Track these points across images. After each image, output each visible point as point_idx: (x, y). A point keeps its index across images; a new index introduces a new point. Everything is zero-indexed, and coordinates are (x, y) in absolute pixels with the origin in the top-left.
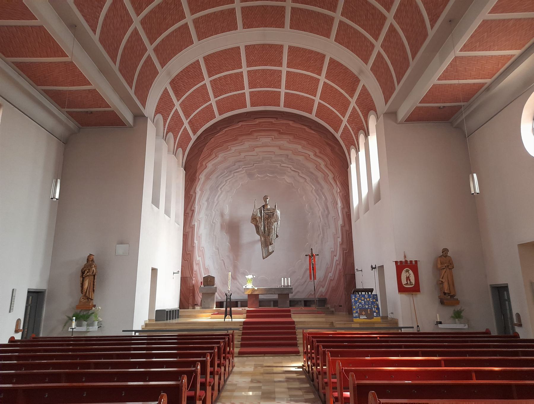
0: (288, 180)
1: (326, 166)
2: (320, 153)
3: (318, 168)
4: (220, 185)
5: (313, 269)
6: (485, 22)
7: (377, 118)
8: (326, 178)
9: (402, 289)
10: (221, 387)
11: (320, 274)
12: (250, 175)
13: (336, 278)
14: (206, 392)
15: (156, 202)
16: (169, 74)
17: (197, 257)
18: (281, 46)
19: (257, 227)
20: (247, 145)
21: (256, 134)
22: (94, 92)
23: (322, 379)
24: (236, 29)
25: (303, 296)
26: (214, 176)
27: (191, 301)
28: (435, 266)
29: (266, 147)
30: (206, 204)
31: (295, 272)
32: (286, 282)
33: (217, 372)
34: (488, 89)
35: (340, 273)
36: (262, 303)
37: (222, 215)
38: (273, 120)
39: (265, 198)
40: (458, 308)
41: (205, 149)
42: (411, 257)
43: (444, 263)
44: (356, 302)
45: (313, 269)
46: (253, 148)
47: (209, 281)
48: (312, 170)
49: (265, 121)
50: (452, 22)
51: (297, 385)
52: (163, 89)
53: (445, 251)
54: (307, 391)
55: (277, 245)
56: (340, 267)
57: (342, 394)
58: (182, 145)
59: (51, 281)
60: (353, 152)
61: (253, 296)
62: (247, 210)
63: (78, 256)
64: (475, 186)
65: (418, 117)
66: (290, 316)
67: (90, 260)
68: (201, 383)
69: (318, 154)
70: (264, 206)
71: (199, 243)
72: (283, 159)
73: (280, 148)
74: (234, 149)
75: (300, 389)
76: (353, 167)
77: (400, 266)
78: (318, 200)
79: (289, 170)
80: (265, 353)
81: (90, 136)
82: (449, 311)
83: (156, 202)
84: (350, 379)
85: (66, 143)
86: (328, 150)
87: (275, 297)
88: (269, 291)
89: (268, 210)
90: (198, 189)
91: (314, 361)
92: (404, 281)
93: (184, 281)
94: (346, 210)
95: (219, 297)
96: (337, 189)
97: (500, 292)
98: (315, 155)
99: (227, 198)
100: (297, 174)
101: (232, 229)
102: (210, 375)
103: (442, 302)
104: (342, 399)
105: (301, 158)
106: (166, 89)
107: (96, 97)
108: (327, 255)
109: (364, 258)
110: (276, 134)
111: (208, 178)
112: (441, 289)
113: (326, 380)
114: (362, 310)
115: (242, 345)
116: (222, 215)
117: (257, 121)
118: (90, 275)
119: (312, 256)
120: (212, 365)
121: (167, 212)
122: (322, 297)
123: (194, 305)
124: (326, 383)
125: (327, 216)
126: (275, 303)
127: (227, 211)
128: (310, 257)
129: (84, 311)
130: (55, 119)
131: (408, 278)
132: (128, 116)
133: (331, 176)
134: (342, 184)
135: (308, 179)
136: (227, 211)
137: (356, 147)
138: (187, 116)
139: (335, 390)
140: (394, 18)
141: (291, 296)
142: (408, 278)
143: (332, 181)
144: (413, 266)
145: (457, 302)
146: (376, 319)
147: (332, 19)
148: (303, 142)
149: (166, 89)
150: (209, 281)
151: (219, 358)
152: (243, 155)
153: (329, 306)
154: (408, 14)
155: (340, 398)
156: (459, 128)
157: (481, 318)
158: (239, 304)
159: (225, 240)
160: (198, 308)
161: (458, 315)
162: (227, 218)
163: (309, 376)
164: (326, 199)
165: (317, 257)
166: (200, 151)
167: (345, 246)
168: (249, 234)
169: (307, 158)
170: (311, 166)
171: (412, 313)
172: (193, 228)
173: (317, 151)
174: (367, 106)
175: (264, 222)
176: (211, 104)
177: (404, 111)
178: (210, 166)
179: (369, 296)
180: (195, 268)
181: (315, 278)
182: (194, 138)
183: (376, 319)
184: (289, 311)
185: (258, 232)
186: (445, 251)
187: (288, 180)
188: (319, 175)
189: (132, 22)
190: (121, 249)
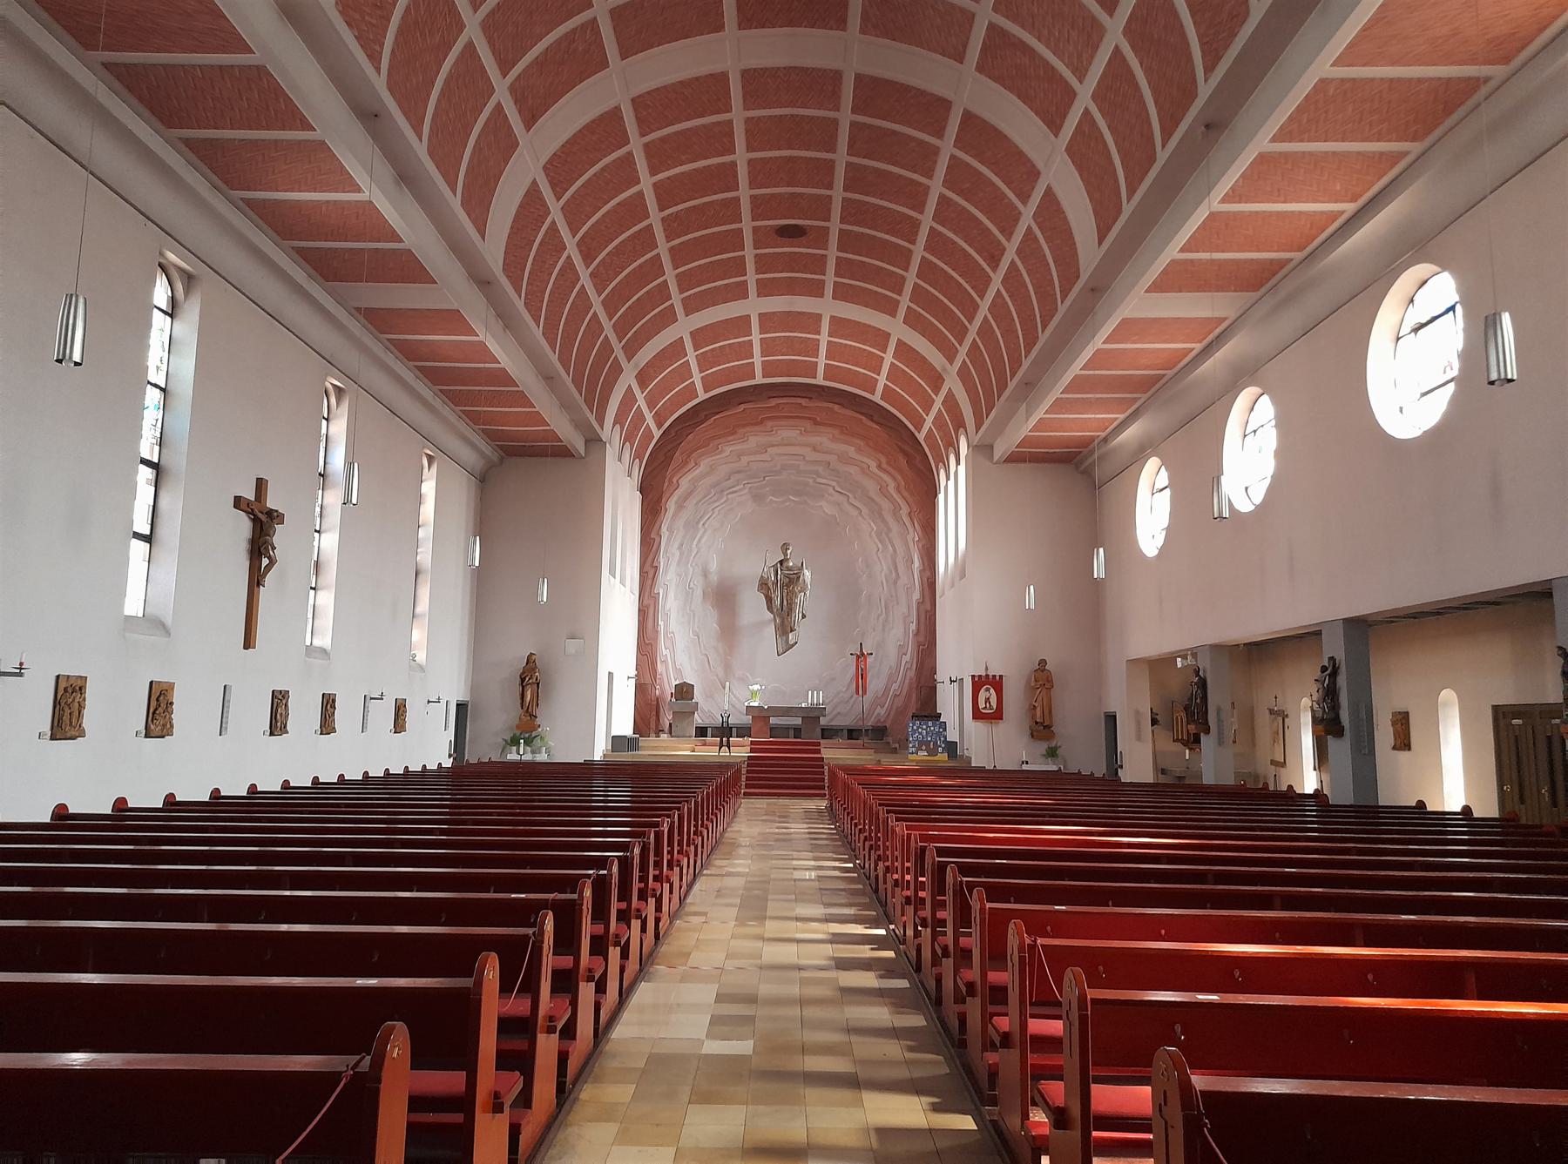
0: (829, 509)
1: (898, 489)
2: (888, 463)
5: (861, 675)
6: (1262, 158)
8: (896, 509)
9: (978, 715)
10: (573, 1065)
11: (875, 684)
12: (758, 498)
14: (606, 960)
15: (612, 573)
16: (636, 365)
17: (663, 650)
18: (820, 316)
19: (769, 600)
20: (753, 441)
21: (770, 424)
22: (260, 73)
23: (987, 1018)
24: (720, 28)
25: (846, 721)
26: (692, 501)
27: (653, 725)
28: (1028, 682)
29: (787, 445)
30: (677, 554)
32: (814, 698)
33: (617, 936)
34: (1105, 440)
36: (774, 731)
38: (804, 402)
39: (785, 548)
42: (995, 671)
43: (1042, 679)
44: (914, 732)
45: (861, 675)
46: (763, 449)
47: (684, 691)
48: (872, 494)
49: (789, 399)
50: (1213, 126)
51: (881, 1014)
52: (527, 183)
53: (1043, 662)
54: (886, 969)
55: (806, 632)
56: (912, 673)
57: (1024, 1026)
58: (638, 455)
59: (474, 688)
61: (760, 715)
62: (755, 564)
63: (514, 654)
64: (1099, 571)
65: (1028, 456)
66: (819, 752)
67: (530, 659)
68: (592, 937)
69: (884, 466)
70: (781, 562)
71: (666, 626)
72: (820, 469)
73: (815, 449)
74: (728, 450)
75: (880, 993)
76: (941, 497)
78: (880, 552)
80: (779, 795)
81: (519, 469)
82: (1042, 747)
83: (612, 573)
84: (975, 905)
85: (485, 481)
86: (903, 462)
87: (798, 721)
88: (787, 712)
89: (789, 569)
90: (664, 529)
91: (927, 913)
92: (982, 704)
93: (641, 690)
95: (698, 720)
96: (914, 535)
98: (879, 467)
99: (718, 538)
101: (723, 598)
102: (554, 990)
104: (1023, 1043)
105: (853, 470)
106: (534, 182)
107: (369, 222)
108: (892, 651)
109: (956, 661)
110: (808, 424)
111: (680, 506)
112: (1034, 716)
113: (1004, 1024)
114: (922, 744)
115: (747, 786)
116: (705, 574)
117: (773, 402)
118: (531, 681)
119: (861, 656)
120: (600, 913)
121: (623, 582)
123: (658, 732)
124: (970, 986)
125: (895, 583)
126: (797, 731)
127: (714, 567)
129: (526, 730)
130: (471, 450)
131: (987, 700)
132: (579, 445)
133: (905, 510)
134: (923, 527)
135: (865, 511)
136: (714, 567)
138: (643, 388)
139: (999, 1009)
140: (1094, 97)
141: (823, 721)
142: (987, 700)
143: (906, 519)
144: (997, 683)
147: (936, 151)
149: (534, 182)
150: (684, 691)
151: (624, 895)
152: (745, 459)
153: (890, 739)
154: (1152, 29)
155: (1017, 1037)
156: (1088, 473)
157: (1085, 758)
160: (664, 736)
161: (1052, 753)
162: (714, 578)
163: (830, 808)
165: (870, 660)
166: (669, 458)
167: (921, 639)
168: (753, 608)
169: (865, 471)
170: (871, 487)
171: (993, 747)
172: (656, 598)
173: (884, 460)
175: (781, 591)
176: (640, 194)
177: (1002, 448)
178: (685, 483)
180: (660, 668)
181: (864, 692)
182: (657, 434)
185: (770, 608)
186: (1043, 662)
187: (829, 509)
188: (886, 505)
189: (461, 27)
190: (572, 646)
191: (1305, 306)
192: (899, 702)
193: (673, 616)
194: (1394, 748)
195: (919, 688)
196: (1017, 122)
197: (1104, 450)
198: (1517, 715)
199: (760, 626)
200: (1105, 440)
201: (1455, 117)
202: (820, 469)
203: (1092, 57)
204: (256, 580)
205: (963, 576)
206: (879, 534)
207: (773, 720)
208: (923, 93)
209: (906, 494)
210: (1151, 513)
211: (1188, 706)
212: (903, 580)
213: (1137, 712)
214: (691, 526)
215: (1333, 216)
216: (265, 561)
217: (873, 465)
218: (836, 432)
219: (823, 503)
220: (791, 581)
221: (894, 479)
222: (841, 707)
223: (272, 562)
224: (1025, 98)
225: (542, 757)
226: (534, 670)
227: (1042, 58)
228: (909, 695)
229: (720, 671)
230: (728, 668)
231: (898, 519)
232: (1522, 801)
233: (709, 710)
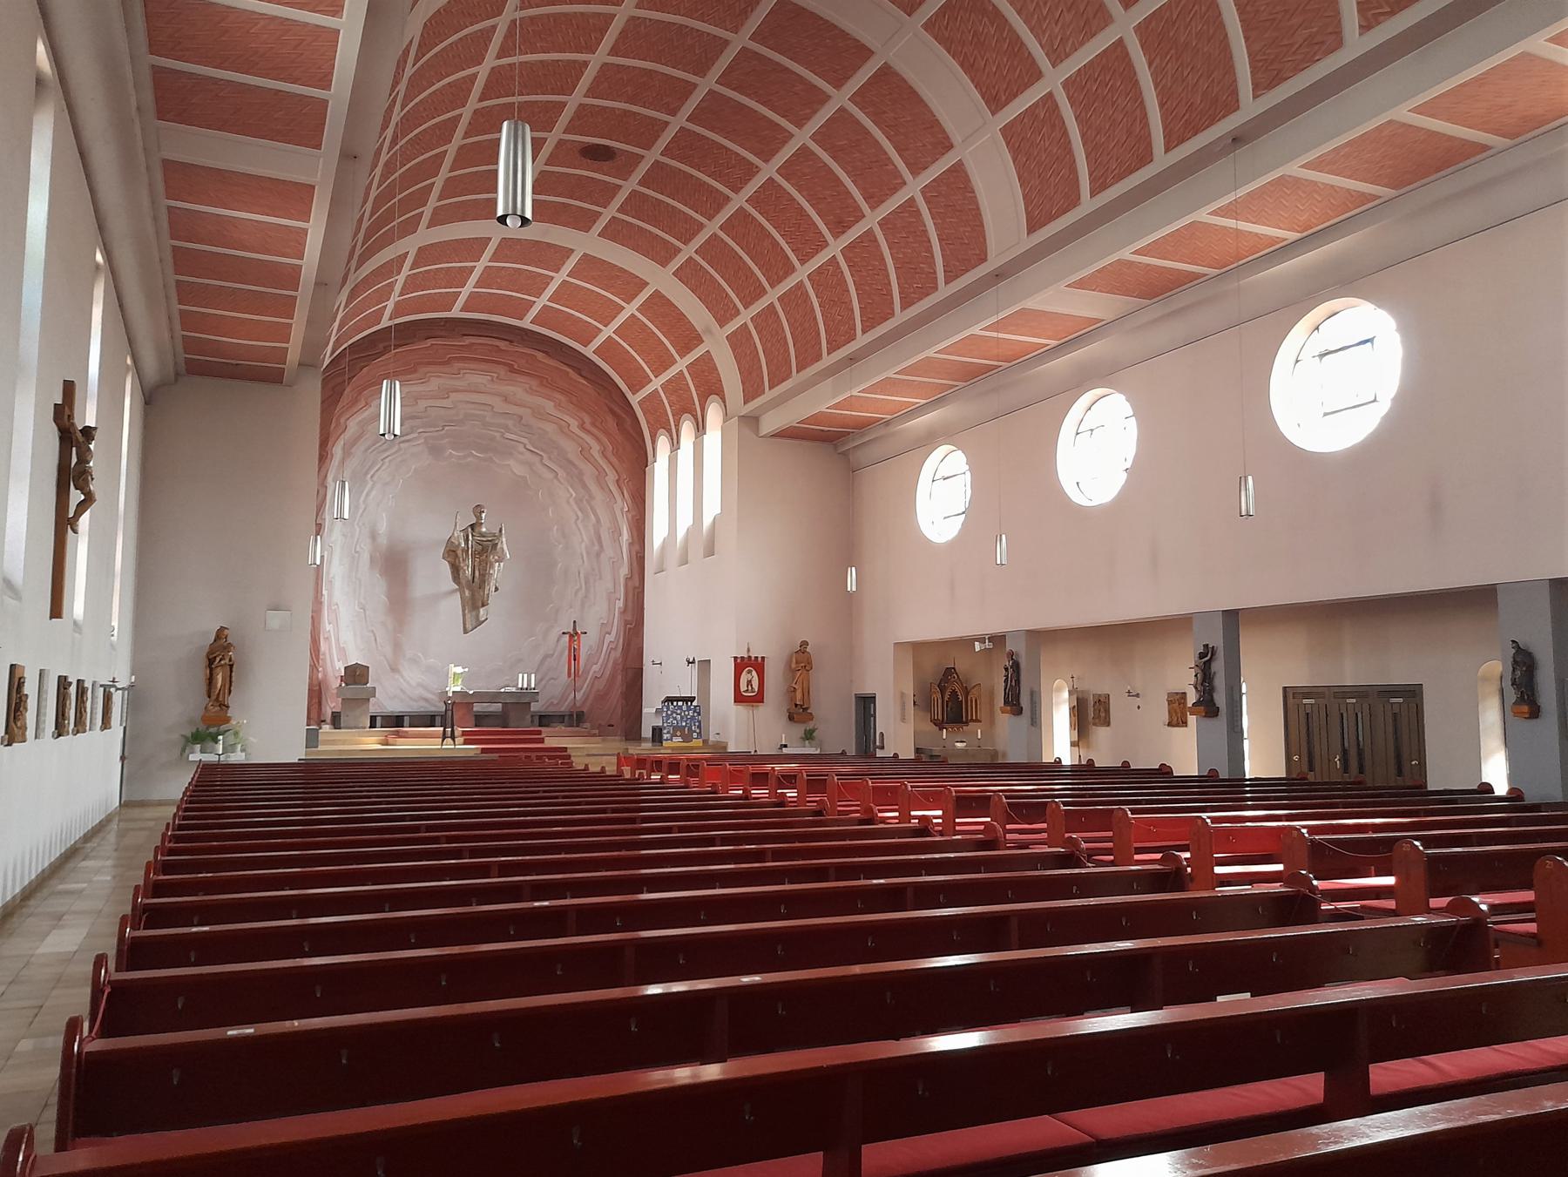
0: (519, 470)
2: (593, 424)
3: (584, 452)
4: (370, 468)
7: (727, 417)
8: (600, 477)
9: (739, 698)
12: (435, 451)
13: (608, 672)
17: (327, 626)
19: (456, 570)
20: (435, 384)
28: (789, 663)
29: (478, 392)
31: (520, 660)
35: (615, 663)
37: (374, 536)
38: (503, 345)
39: (478, 510)
40: (810, 725)
41: (348, 390)
43: (801, 661)
46: (446, 393)
47: (356, 675)
48: (571, 456)
53: (804, 644)
55: (496, 609)
60: (663, 443)
62: (435, 528)
64: (851, 585)
67: (220, 634)
69: (588, 425)
71: (330, 595)
72: (510, 423)
73: (506, 400)
77: (741, 665)
78: (577, 518)
79: (521, 448)
86: (611, 423)
88: (493, 697)
92: (743, 687)
94: (637, 547)
95: (374, 708)
96: (622, 505)
97: (866, 704)
98: (582, 427)
100: (537, 459)
101: (394, 565)
103: (791, 718)
105: (549, 428)
110: (502, 371)
111: (347, 453)
112: (792, 699)
116: (374, 536)
117: (468, 341)
118: (220, 663)
122: (552, 709)
125: (598, 555)
127: (383, 528)
128: (571, 636)
131: (749, 682)
133: (611, 477)
134: (633, 497)
135: (561, 473)
136: (383, 528)
137: (669, 431)
141: (534, 707)
142: (749, 682)
144: (758, 665)
145: (811, 717)
146: (697, 743)
148: (558, 396)
152: (422, 404)
153: (587, 725)
154: (1182, 37)
158: (406, 720)
159: (378, 589)
161: (809, 736)
162: (383, 541)
164: (598, 521)
168: (432, 577)
169: (564, 430)
170: (571, 449)
171: (734, 727)
173: (587, 419)
174: (711, 386)
175: (471, 563)
179: (689, 709)
183: (697, 743)
184: (539, 733)
186: (804, 644)
187: (519, 470)
188: (588, 469)
190: (275, 620)
191: (1206, 313)
192: (600, 685)
193: (338, 584)
194: (1170, 724)
195: (625, 669)
196: (948, 91)
197: (882, 432)
198: (1307, 695)
199: (437, 598)
200: (888, 423)
201: (1443, 173)
202: (510, 423)
203: (1082, 44)
204: (64, 524)
205: (710, 551)
206: (578, 501)
207: (477, 708)
208: (844, 35)
209: (614, 460)
210: (942, 494)
211: (948, 692)
212: (609, 551)
213: (902, 694)
214: (359, 480)
215: (1273, 241)
216: (76, 496)
217: (574, 424)
218: (534, 383)
219: (511, 462)
220: (486, 549)
221: (597, 439)
222: (555, 692)
223: (89, 500)
224: (968, 66)
225: (237, 757)
226: (228, 647)
227: (1012, 30)
228: (613, 677)
229: (388, 650)
230: (397, 646)
231: (602, 485)
232: (1311, 769)
233: (387, 700)
